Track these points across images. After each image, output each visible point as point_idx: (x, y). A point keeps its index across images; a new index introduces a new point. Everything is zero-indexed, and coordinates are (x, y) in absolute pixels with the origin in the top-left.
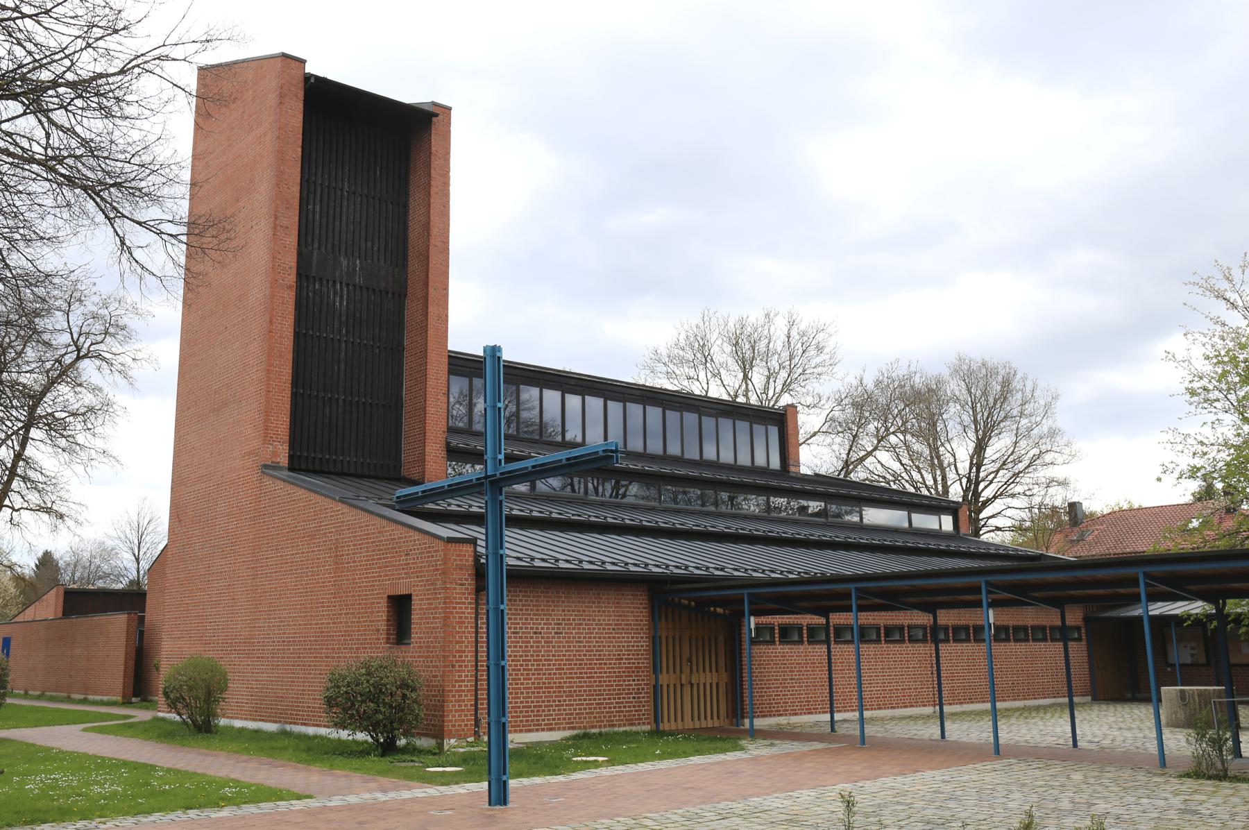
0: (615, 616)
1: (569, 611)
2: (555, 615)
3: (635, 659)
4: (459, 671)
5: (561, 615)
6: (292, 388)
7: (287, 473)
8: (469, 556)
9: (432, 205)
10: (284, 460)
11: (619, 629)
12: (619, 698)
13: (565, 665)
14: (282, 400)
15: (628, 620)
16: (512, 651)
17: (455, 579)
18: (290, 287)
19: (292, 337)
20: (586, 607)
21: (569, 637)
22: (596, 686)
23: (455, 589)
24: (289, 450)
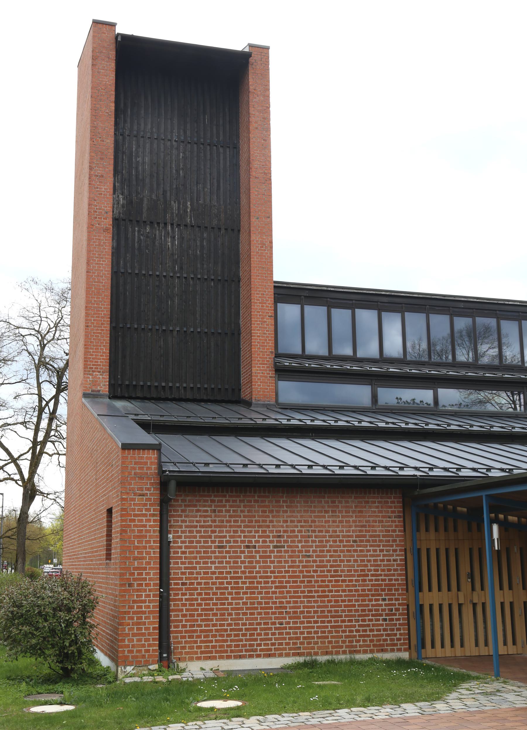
0: (356, 526)
1: (292, 521)
2: (274, 526)
3: (385, 575)
4: (138, 590)
5: (282, 526)
6: (111, 322)
7: (107, 400)
8: (151, 463)
9: (251, 140)
10: (104, 387)
11: (362, 541)
12: (364, 620)
13: (287, 582)
14: (101, 333)
15: (376, 531)
16: (216, 568)
17: (133, 489)
18: (106, 230)
19: (110, 276)
20: (315, 517)
21: (293, 551)
22: (332, 606)
23: (134, 500)
24: (110, 378)
